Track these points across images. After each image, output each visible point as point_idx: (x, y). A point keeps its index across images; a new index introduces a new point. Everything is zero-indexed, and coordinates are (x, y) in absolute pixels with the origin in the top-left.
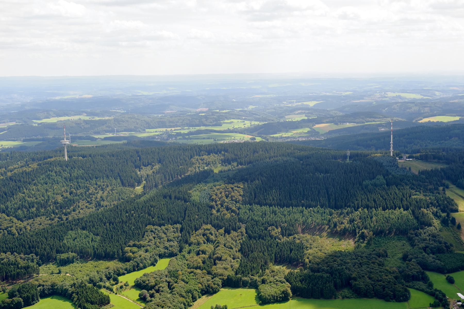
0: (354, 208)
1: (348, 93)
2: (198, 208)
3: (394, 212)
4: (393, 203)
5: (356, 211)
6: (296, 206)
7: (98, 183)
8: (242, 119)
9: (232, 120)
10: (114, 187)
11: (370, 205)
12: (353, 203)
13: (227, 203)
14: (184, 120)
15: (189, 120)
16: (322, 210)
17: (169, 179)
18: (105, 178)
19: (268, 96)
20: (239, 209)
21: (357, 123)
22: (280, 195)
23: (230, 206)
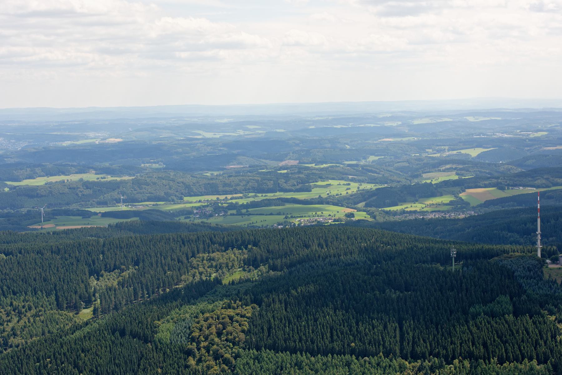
0: (446, 358)
1: (539, 134)
2: (164, 354)
3: (520, 366)
4: (520, 350)
5: (448, 363)
6: (339, 353)
7: (14, 303)
8: (348, 179)
9: (330, 182)
10: (40, 311)
11: (476, 352)
12: (445, 348)
13: (218, 345)
14: (248, 182)
15: (257, 181)
16: (386, 362)
17: (143, 297)
18: (29, 293)
19: (404, 139)
20: (237, 356)
21: (538, 187)
22: (313, 332)
23: (222, 351)
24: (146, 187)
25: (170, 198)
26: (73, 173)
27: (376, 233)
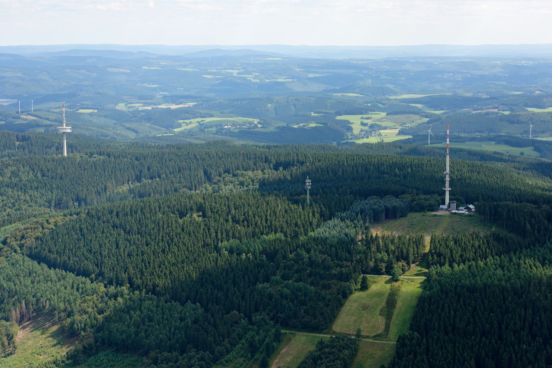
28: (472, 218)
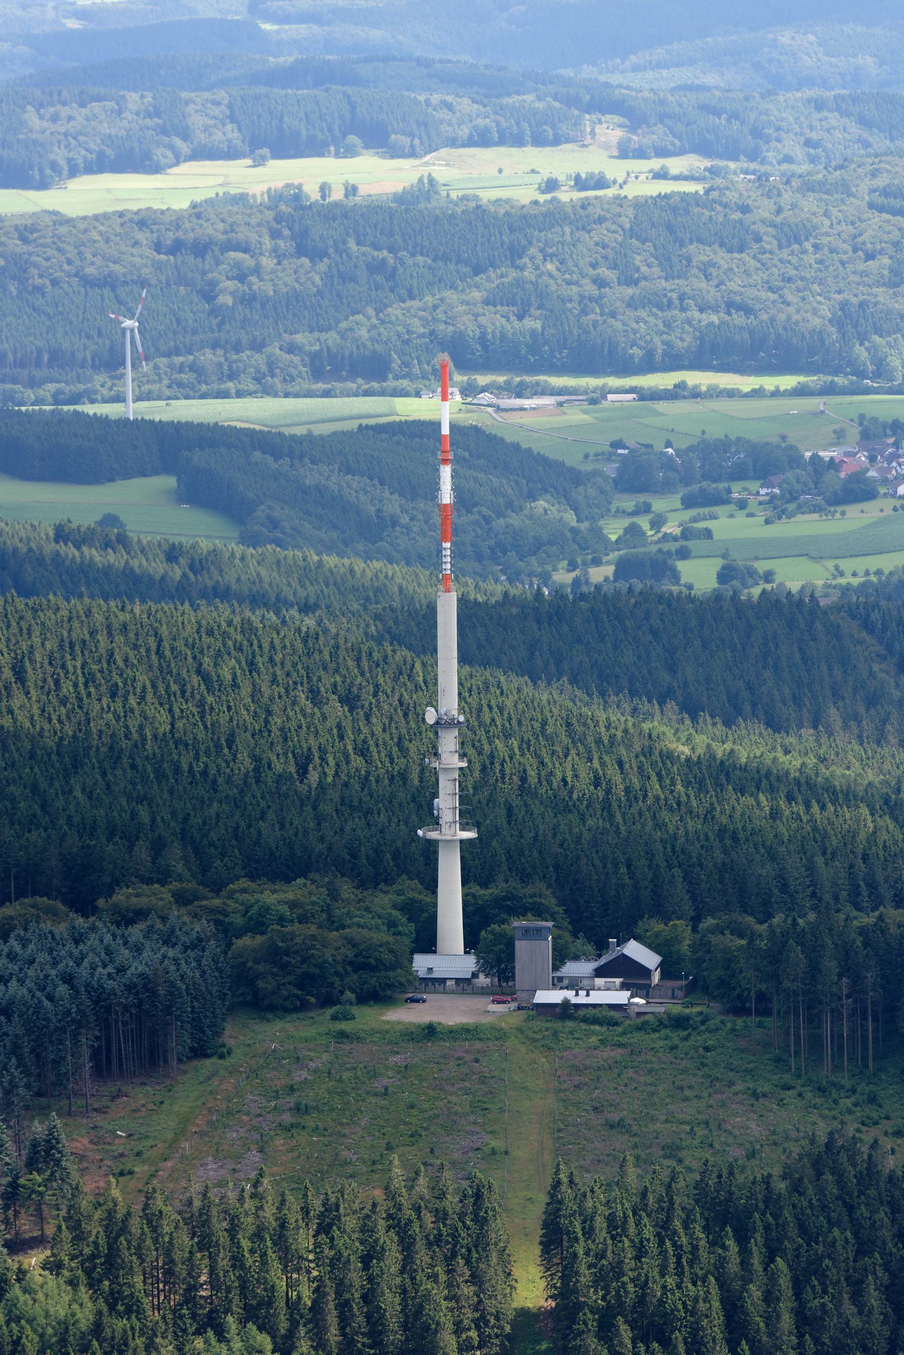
24: (722, 257)
25: (861, 352)
26: (453, 143)
27: (177, 770)
28: (698, 1040)
